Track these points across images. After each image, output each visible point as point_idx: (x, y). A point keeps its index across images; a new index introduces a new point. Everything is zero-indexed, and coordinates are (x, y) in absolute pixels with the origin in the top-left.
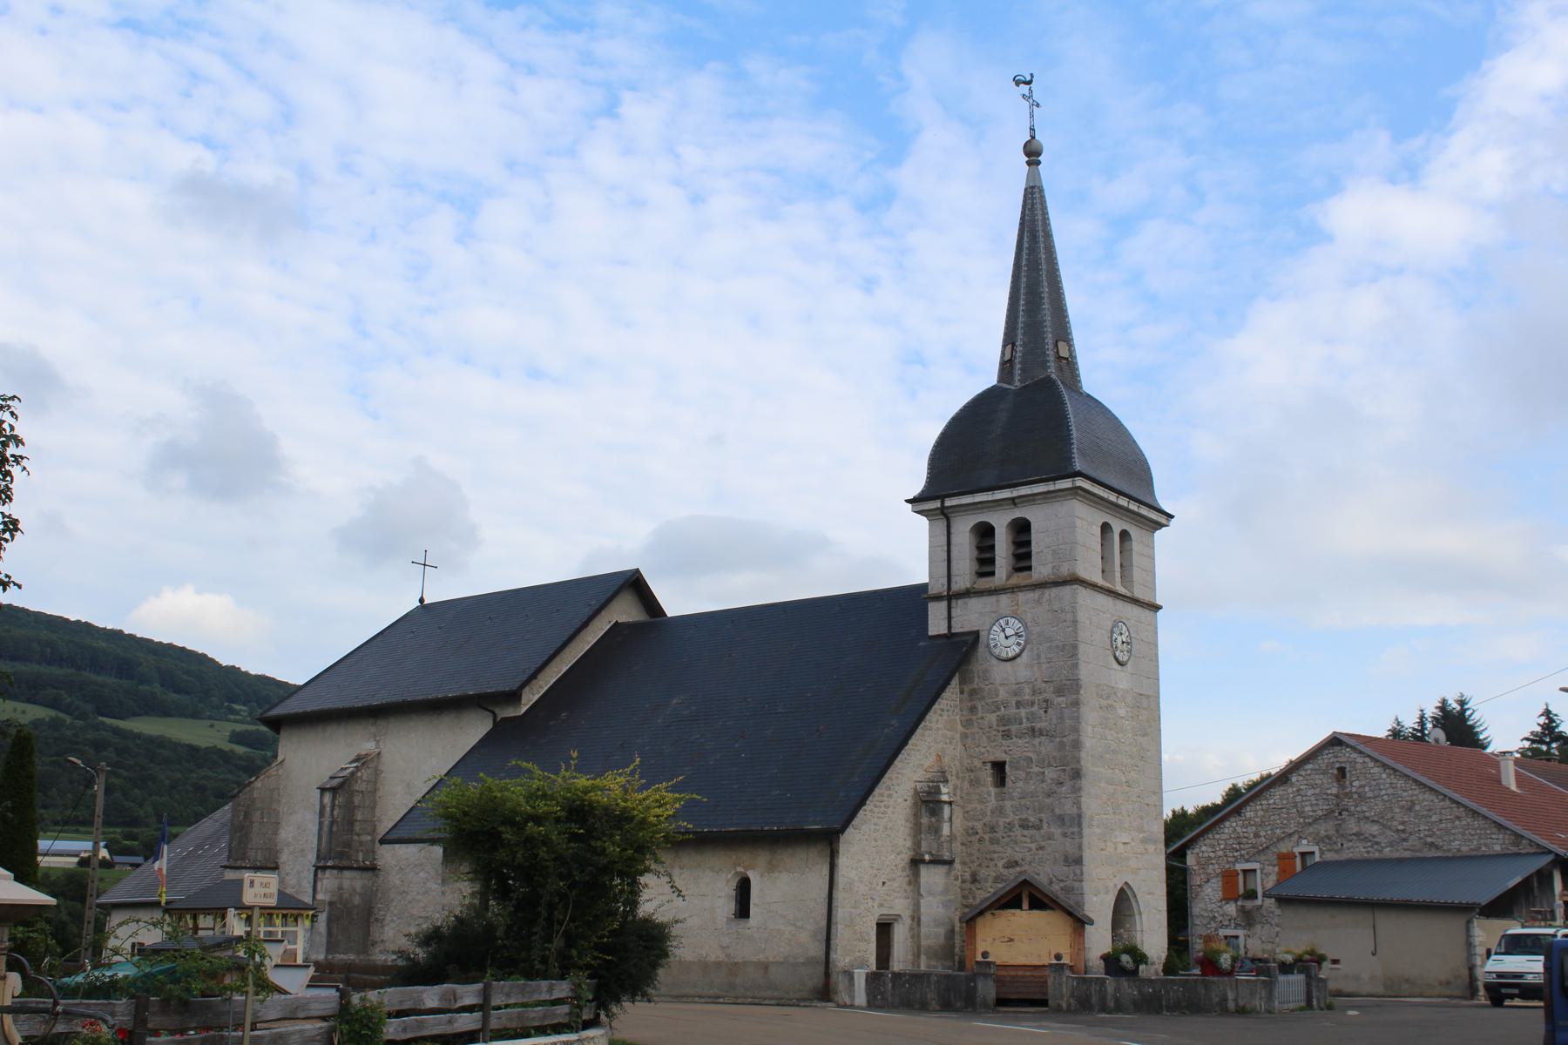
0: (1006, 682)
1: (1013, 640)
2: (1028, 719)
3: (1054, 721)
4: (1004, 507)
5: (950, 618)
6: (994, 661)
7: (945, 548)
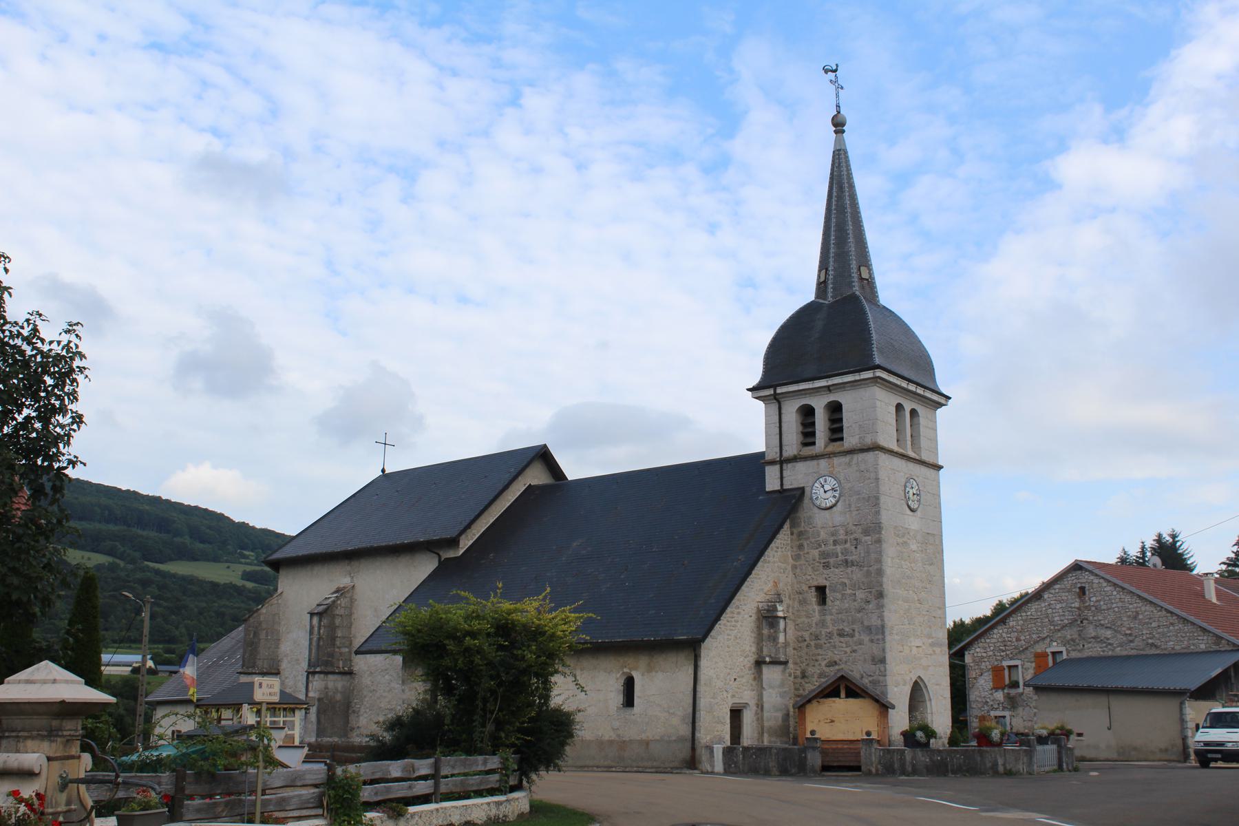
1: (830, 494)
2: (842, 553)
5: (782, 478)
6: (816, 510)
7: (778, 425)
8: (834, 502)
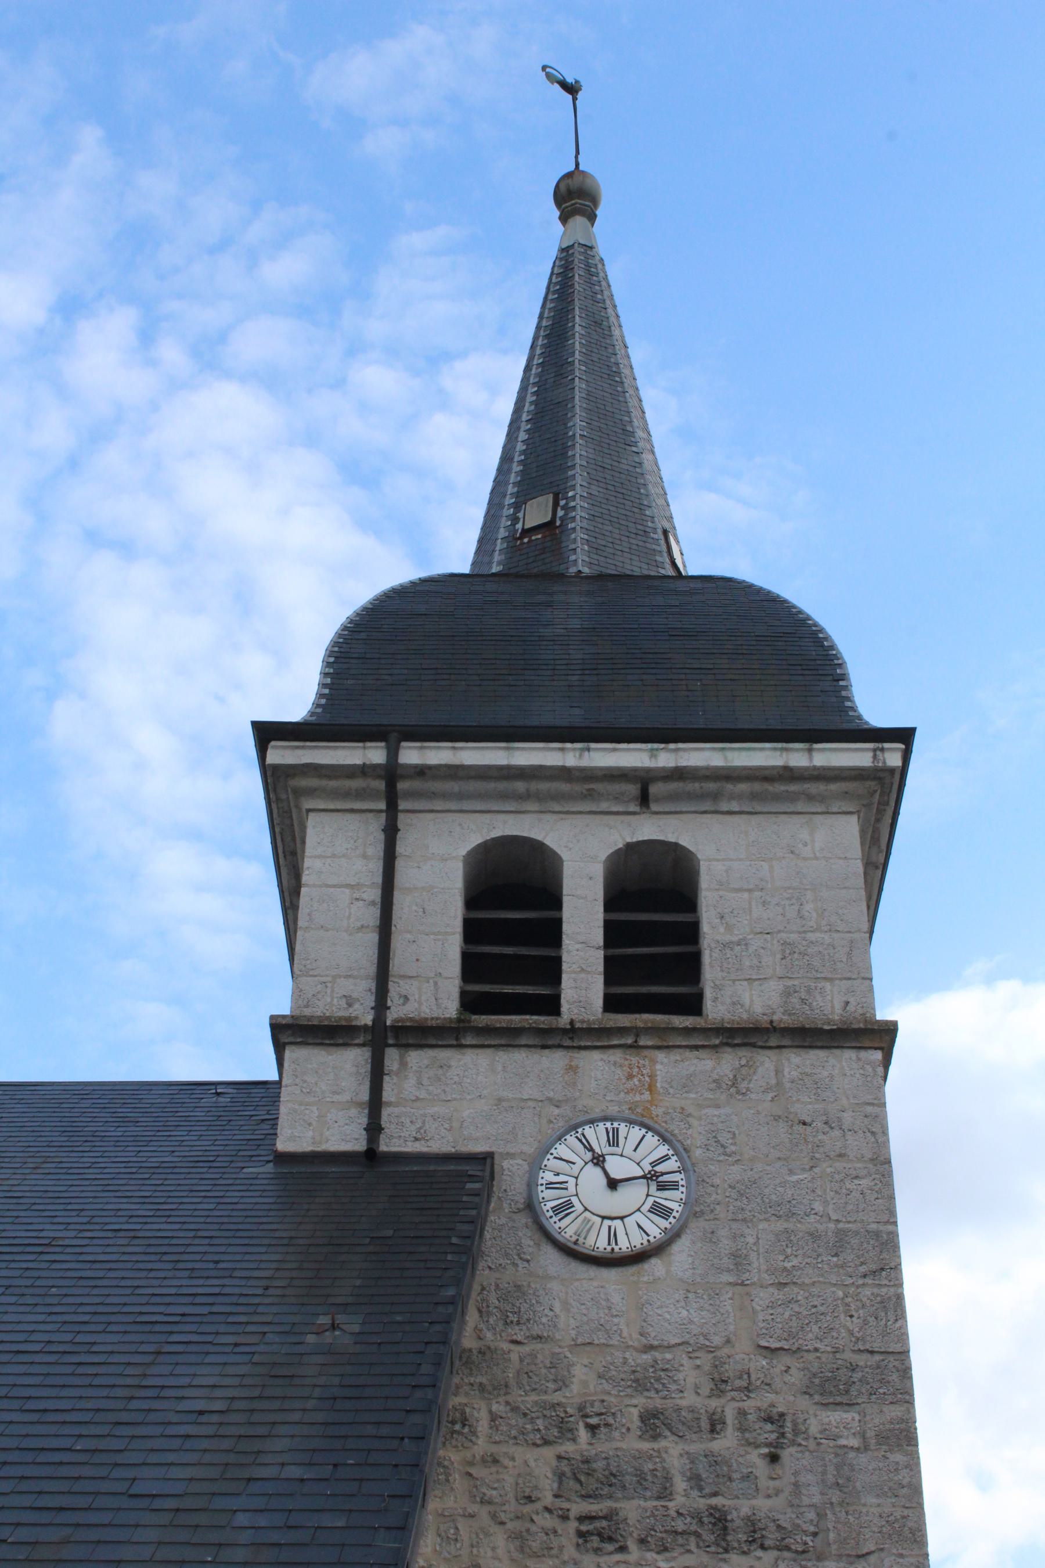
0: (600, 1338)
1: (633, 1196)
2: (695, 1480)
3: (813, 1495)
4: (604, 806)
5: (375, 1104)
6: (551, 1260)
7: (374, 894)
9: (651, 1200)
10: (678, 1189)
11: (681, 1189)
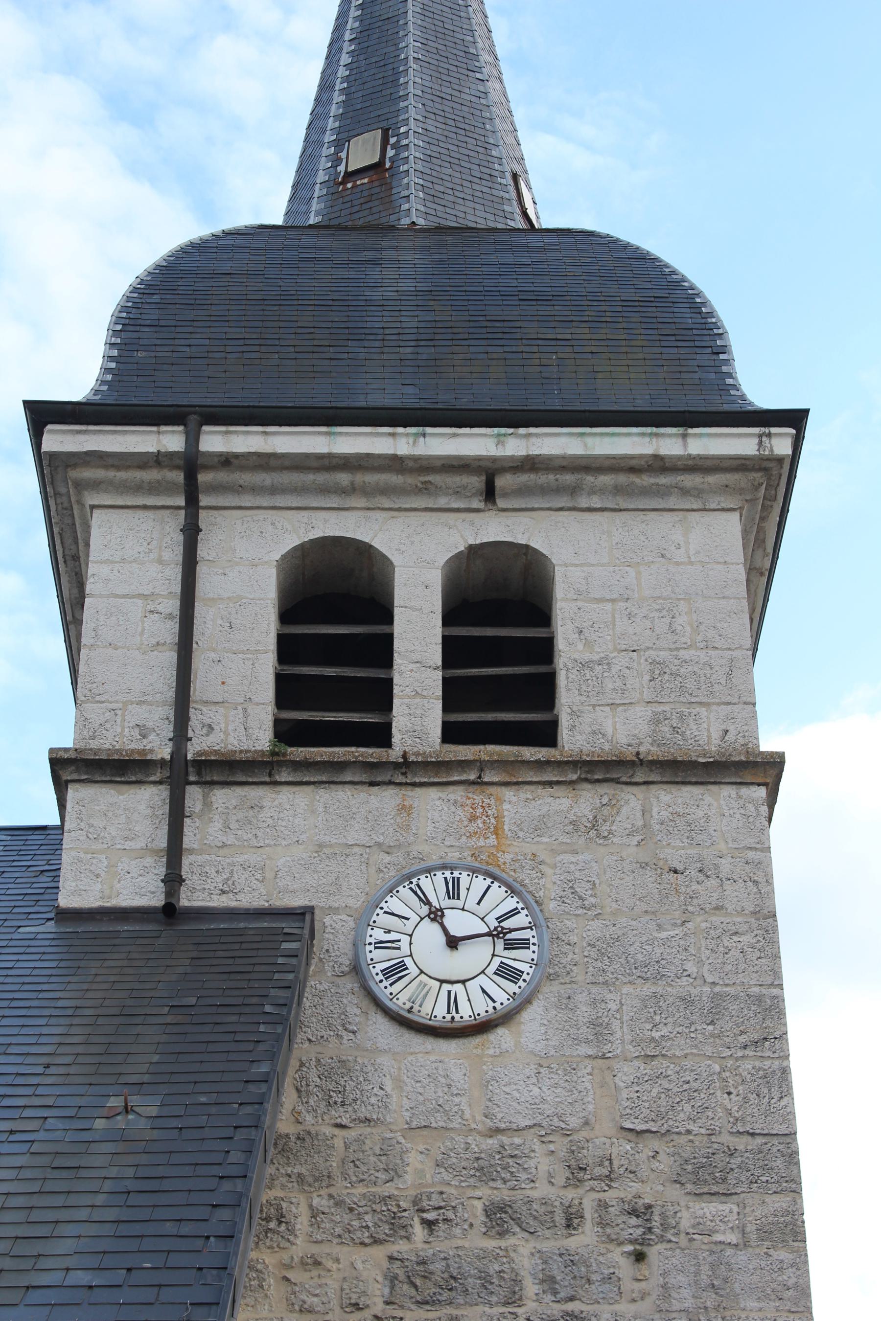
0: (438, 1121)
2: (549, 1282)
4: (442, 502)
7: (173, 606)
8: (501, 997)
9: (497, 961)
10: (529, 948)
11: (532, 948)
